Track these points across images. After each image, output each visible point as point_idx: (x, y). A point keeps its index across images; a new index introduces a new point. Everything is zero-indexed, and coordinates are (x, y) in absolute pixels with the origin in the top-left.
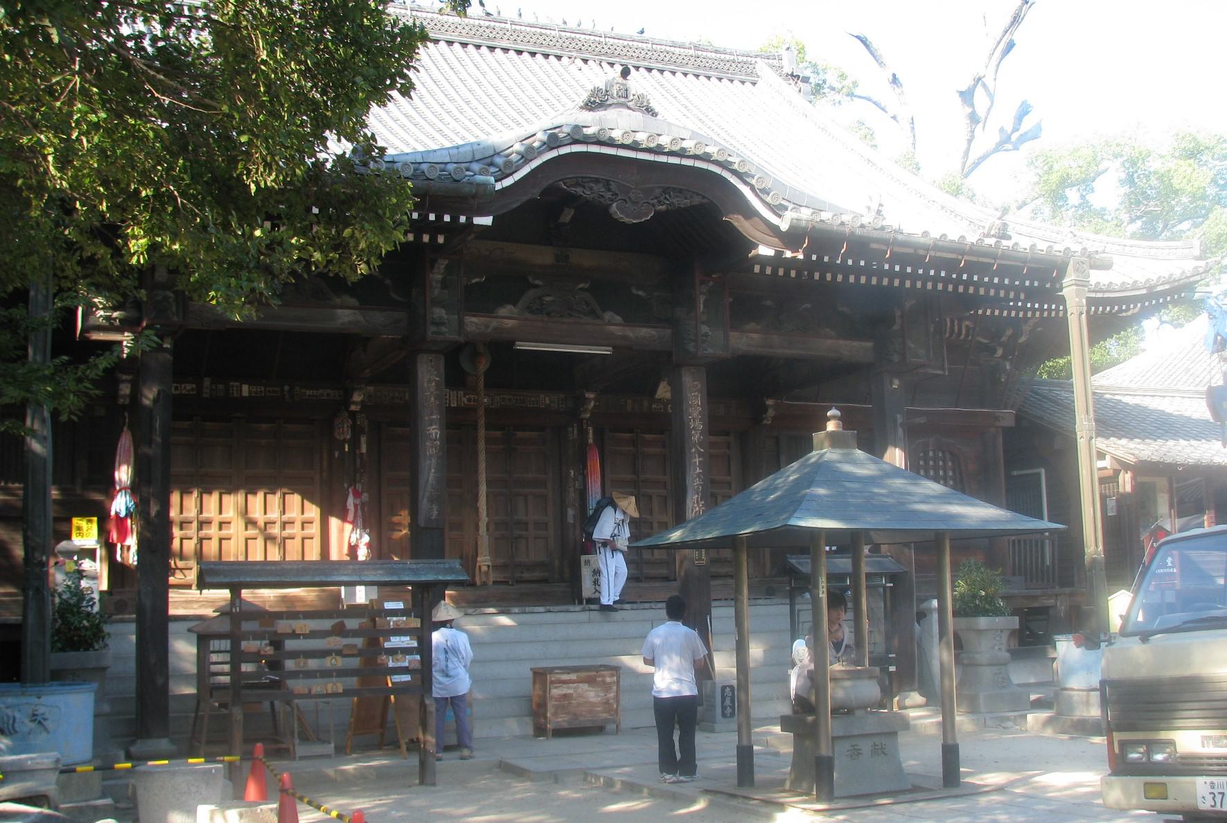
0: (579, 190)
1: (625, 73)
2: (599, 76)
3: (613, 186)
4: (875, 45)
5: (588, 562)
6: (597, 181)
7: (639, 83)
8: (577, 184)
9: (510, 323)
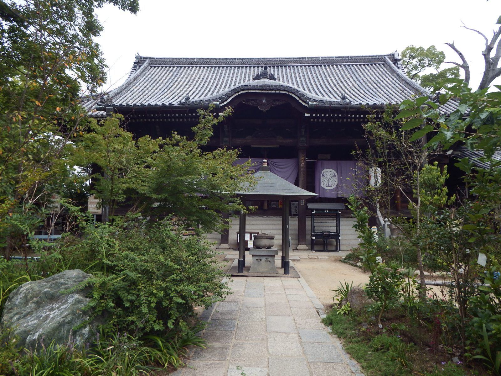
0: (248, 103)
1: (266, 68)
2: (260, 70)
3: (258, 101)
4: (456, 47)
5: (293, 204)
6: (253, 100)
7: (270, 71)
8: (248, 102)
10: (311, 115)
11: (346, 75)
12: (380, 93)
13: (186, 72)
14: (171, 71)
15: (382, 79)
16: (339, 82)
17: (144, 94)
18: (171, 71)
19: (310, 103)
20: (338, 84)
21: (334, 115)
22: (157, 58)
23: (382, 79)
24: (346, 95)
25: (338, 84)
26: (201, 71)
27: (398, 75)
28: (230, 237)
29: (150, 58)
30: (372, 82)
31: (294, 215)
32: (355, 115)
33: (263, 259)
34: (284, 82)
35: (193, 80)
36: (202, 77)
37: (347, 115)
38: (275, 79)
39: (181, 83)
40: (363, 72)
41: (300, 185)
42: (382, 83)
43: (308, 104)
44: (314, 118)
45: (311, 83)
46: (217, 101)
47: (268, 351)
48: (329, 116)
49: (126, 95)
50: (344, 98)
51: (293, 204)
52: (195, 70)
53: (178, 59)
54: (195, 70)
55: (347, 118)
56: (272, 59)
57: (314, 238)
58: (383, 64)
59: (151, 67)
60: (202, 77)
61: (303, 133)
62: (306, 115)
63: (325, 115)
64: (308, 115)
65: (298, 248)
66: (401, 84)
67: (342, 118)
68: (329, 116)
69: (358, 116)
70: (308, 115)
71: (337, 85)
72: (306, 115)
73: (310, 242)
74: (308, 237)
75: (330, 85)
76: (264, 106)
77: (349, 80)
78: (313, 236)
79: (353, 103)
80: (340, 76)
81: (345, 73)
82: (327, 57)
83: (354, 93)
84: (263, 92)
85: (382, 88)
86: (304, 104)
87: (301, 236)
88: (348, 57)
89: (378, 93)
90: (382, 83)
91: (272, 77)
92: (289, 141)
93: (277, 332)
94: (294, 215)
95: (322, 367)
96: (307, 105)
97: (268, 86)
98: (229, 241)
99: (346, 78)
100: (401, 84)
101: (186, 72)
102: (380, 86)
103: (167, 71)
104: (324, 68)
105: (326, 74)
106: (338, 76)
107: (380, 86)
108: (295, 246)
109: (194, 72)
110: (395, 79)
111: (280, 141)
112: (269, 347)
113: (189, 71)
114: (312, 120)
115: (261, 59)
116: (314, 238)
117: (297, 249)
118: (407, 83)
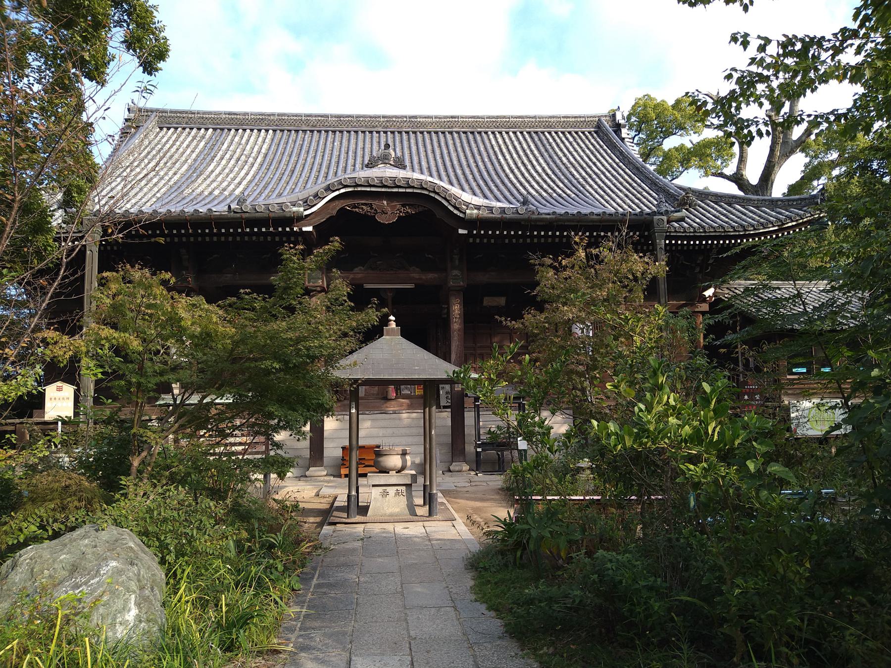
8: (355, 207)
9: (360, 276)
10: (470, 232)
11: (531, 151)
12: (591, 186)
13: (232, 140)
14: (203, 137)
15: (594, 160)
16: (520, 165)
17: (151, 185)
18: (203, 137)
19: (468, 211)
20: (518, 168)
21: (509, 233)
22: (171, 112)
23: (594, 160)
24: (530, 197)
25: (518, 168)
26: (260, 139)
27: (621, 153)
28: (326, 453)
29: (157, 111)
30: (577, 165)
31: (445, 407)
32: (546, 233)
33: (392, 490)
34: (422, 173)
35: (248, 157)
36: (263, 151)
37: (532, 233)
38: (404, 167)
39: (224, 162)
40: (562, 145)
41: (453, 357)
42: (594, 168)
43: (465, 213)
44: (475, 236)
45: (469, 166)
46: (300, 206)
47: (409, 633)
48: (502, 233)
49: (113, 185)
50: (525, 202)
51: (443, 388)
52: (250, 137)
53: (215, 113)
54: (250, 137)
55: (532, 237)
56: (396, 117)
57: (479, 450)
58: (596, 132)
59: (161, 129)
60: (263, 151)
61: (457, 262)
62: (461, 231)
63: (494, 232)
64: (465, 232)
65: (452, 468)
66: (627, 170)
67: (524, 236)
68: (502, 233)
69: (550, 233)
70: (465, 232)
71: (516, 171)
72: (461, 231)
73: (474, 457)
74: (470, 448)
75: (504, 171)
76: (388, 213)
77: (537, 160)
78: (479, 446)
79: (542, 211)
80: (521, 153)
81: (529, 147)
82: (498, 117)
83: (545, 186)
84: (383, 190)
85: (594, 176)
86: (456, 212)
87: (457, 446)
88: (535, 117)
89: (588, 187)
90: (594, 168)
91: (400, 164)
92: (431, 277)
93: (422, 607)
94: (445, 407)
95: (491, 649)
96: (462, 215)
97: (394, 179)
98: (326, 461)
99: (531, 156)
100: (627, 170)
101: (232, 140)
102: (591, 172)
103: (194, 138)
104: (491, 136)
105: (497, 149)
106: (517, 153)
107: (591, 172)
108: (447, 464)
109: (248, 141)
110: (617, 160)
111: (416, 276)
112: (410, 629)
113: (237, 139)
114: (471, 240)
115: (375, 117)
116: (479, 450)
117: (450, 471)
118: (638, 169)
